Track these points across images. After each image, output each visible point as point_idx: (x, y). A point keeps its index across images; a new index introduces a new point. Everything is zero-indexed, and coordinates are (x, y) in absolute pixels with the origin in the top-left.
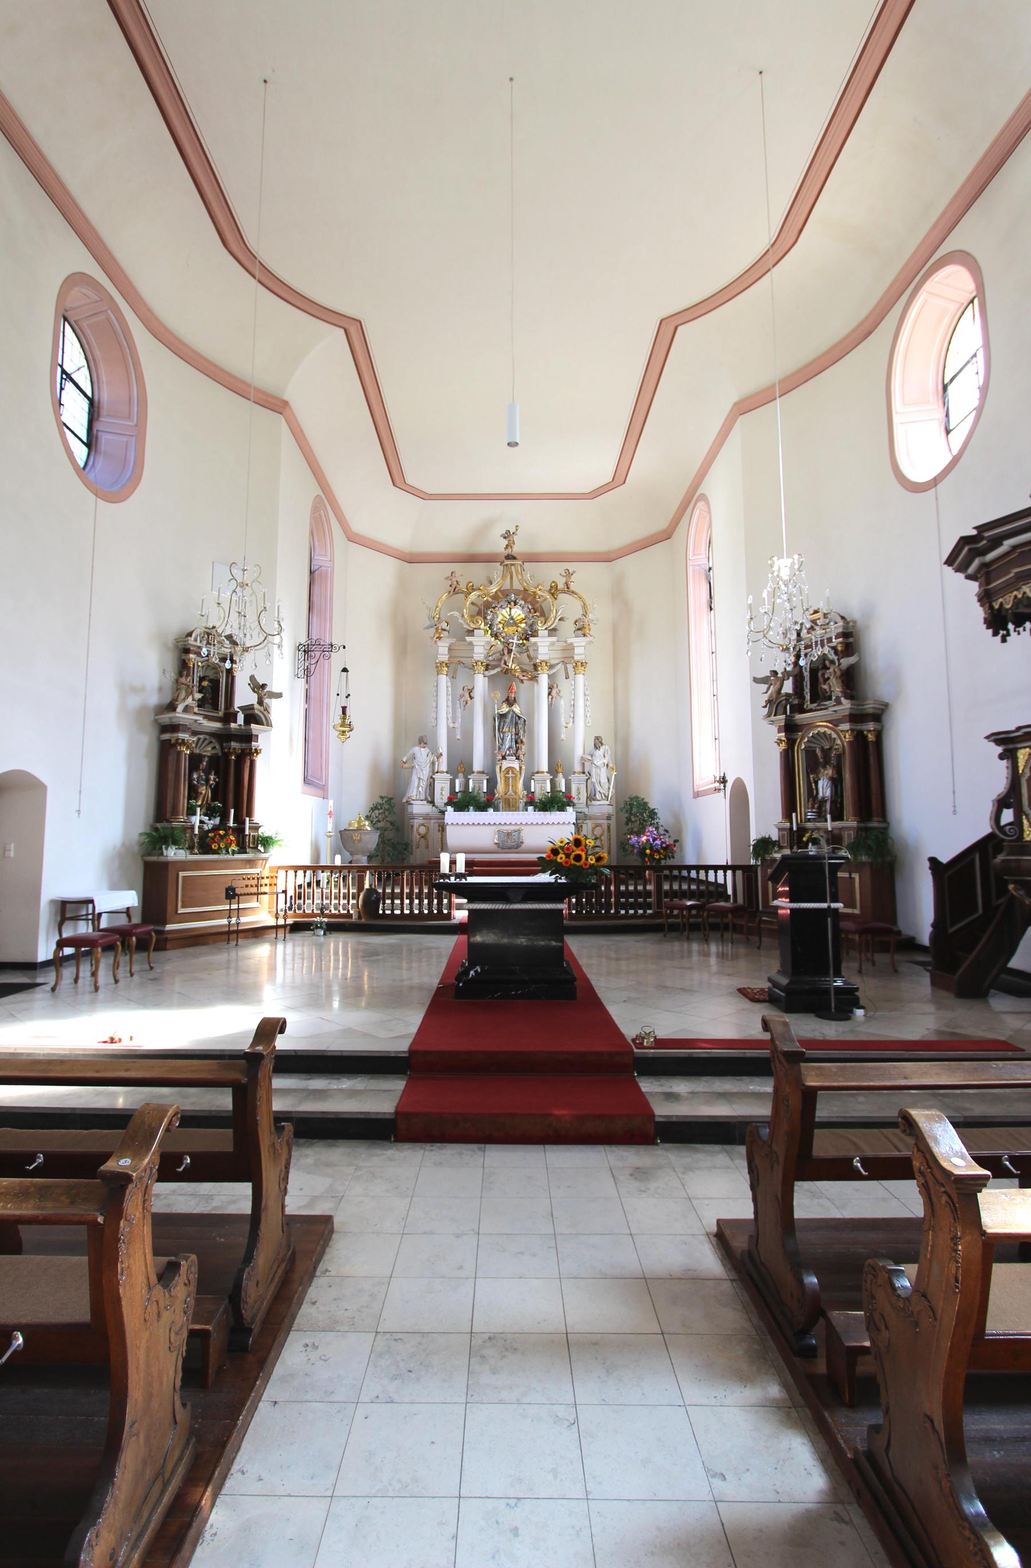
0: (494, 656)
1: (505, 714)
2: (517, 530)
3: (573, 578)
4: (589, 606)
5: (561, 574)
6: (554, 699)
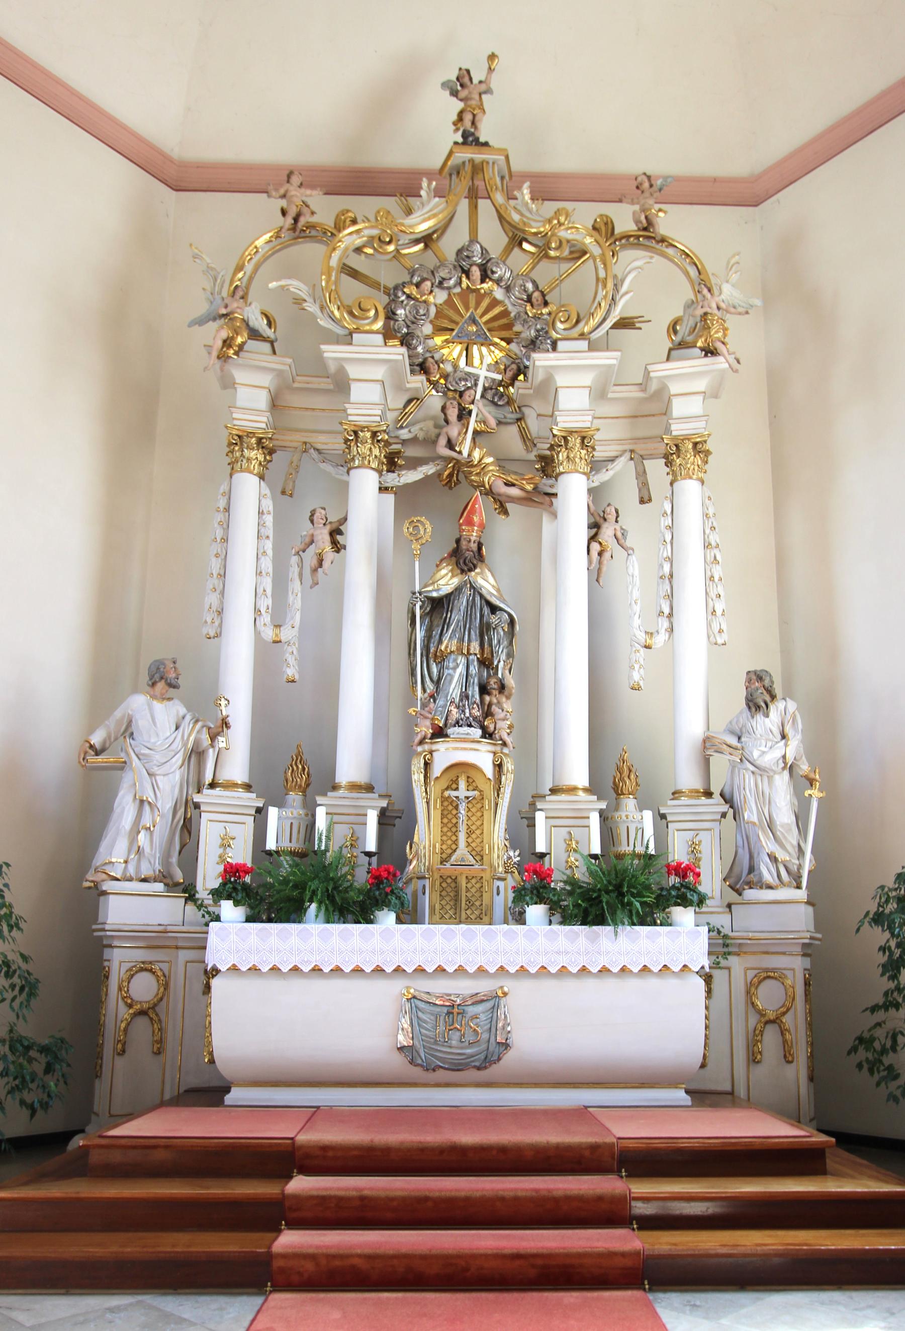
1: (448, 596)
6: (607, 555)
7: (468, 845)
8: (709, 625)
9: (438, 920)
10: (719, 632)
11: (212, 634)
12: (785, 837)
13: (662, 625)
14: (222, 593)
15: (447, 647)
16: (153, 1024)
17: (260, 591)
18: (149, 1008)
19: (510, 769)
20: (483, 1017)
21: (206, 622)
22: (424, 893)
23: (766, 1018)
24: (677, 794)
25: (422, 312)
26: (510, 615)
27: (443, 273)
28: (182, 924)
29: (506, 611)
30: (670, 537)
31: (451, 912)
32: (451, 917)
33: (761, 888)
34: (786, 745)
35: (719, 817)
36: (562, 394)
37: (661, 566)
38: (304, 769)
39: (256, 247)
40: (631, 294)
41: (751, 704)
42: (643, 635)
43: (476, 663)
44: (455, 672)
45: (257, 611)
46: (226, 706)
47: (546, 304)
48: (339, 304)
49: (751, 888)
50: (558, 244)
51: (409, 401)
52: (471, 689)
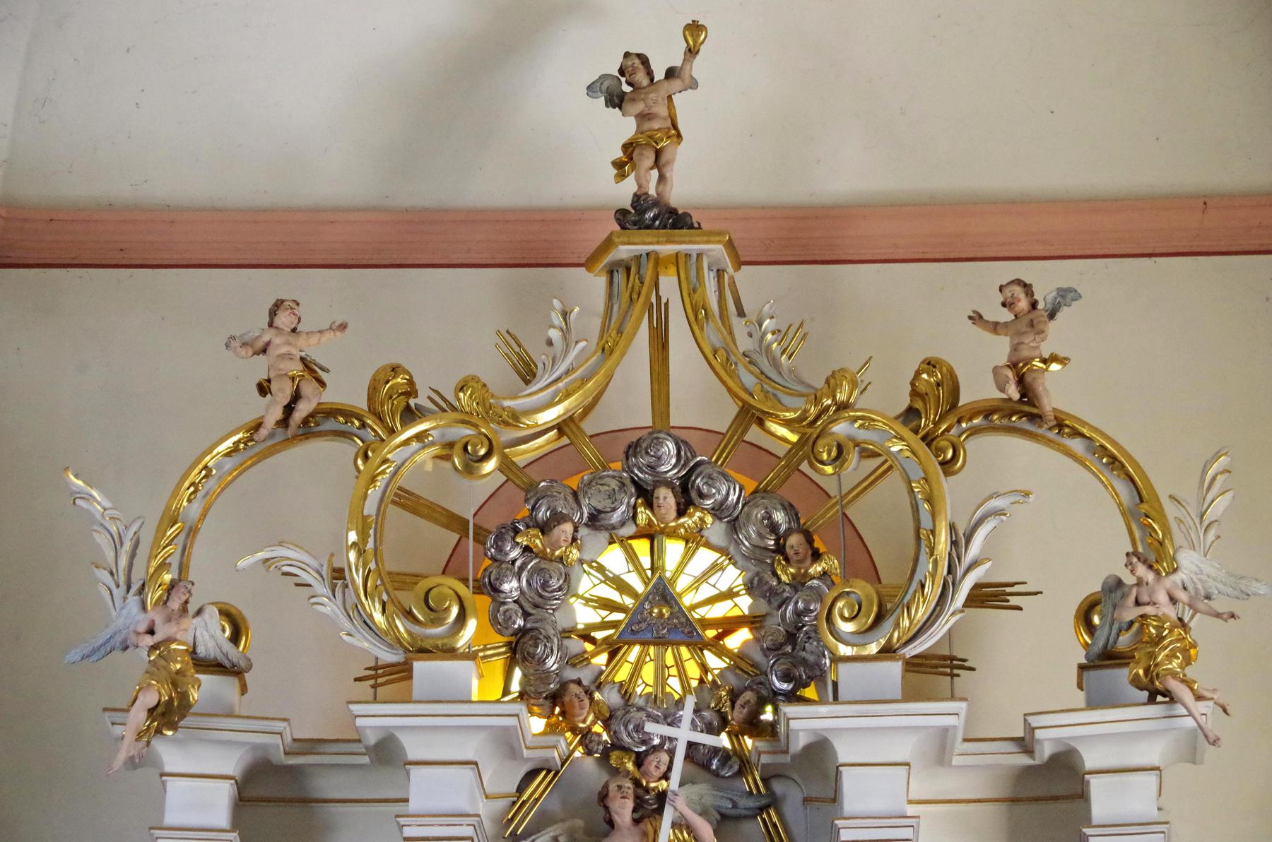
2: (692, 52)
3: (1055, 337)
4: (1170, 510)
5: (976, 318)
25: (555, 583)
27: (599, 502)
39: (206, 467)
40: (988, 565)
48: (385, 597)
50: (834, 454)
51: (531, 775)
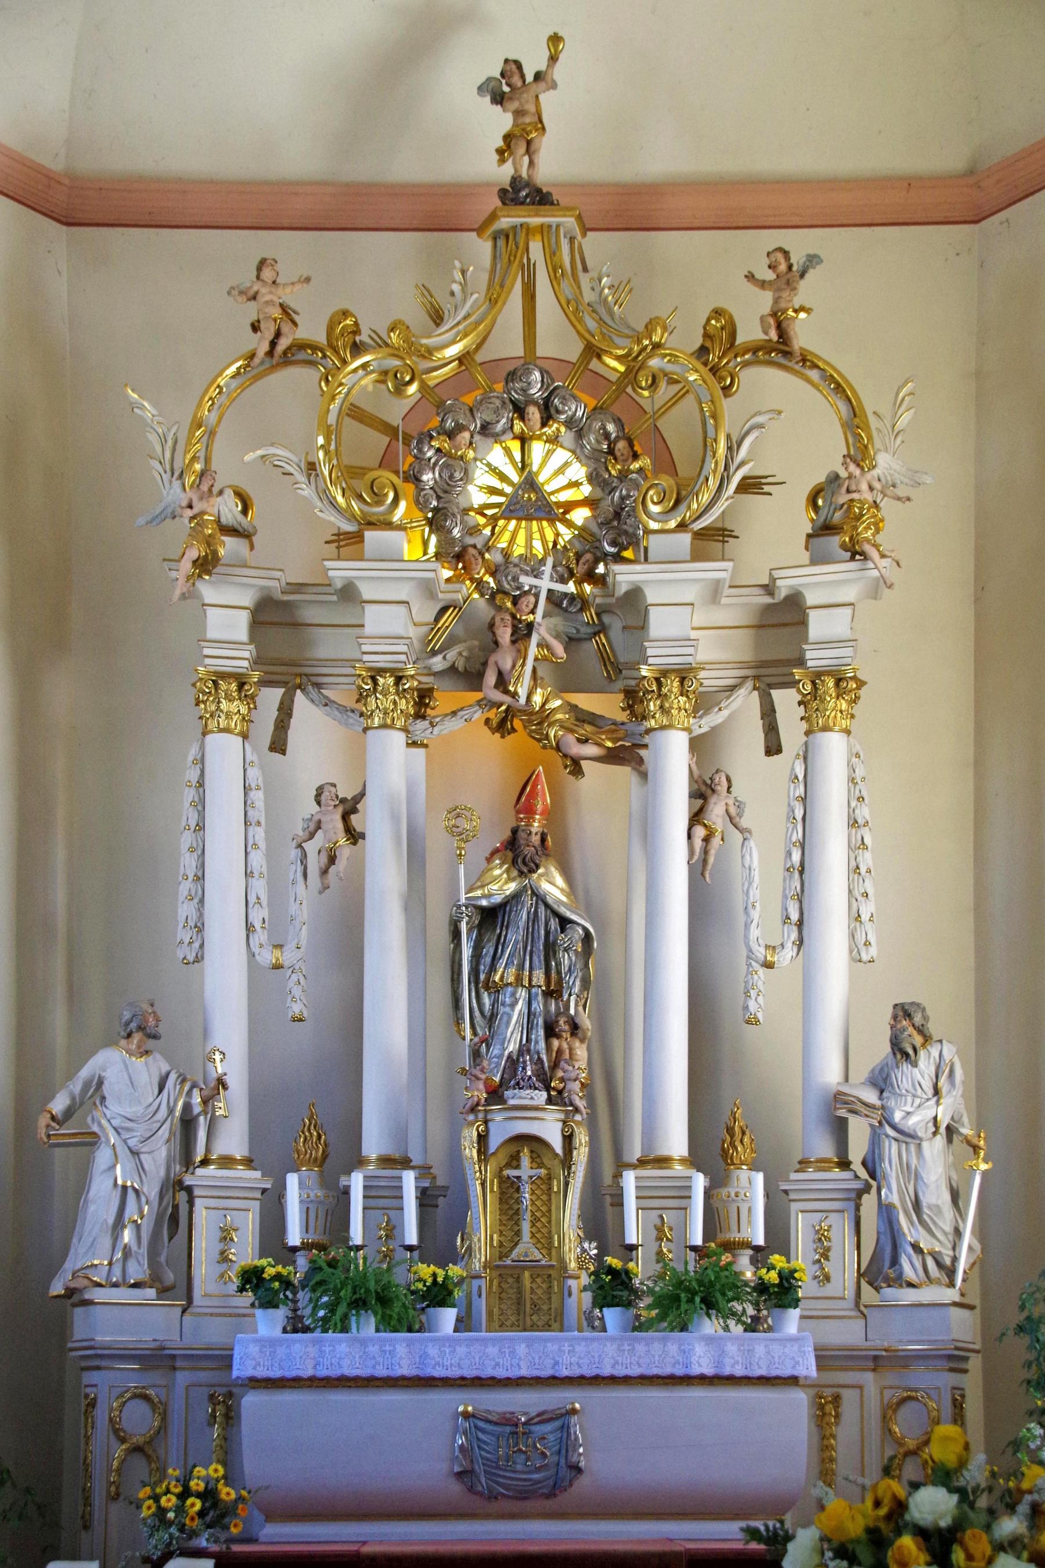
0: (452, 654)
1: (503, 905)
6: (716, 841)
7: (533, 1235)
8: (852, 936)
9: (497, 1327)
10: (865, 944)
11: (191, 958)
12: (935, 1223)
13: (789, 936)
14: (202, 901)
15: (502, 978)
16: (150, 1463)
17: (252, 899)
18: (146, 1443)
19: (583, 1141)
20: (551, 1438)
21: (181, 942)
22: (480, 1296)
23: (905, 1449)
24: (804, 1164)
25: (458, 475)
26: (585, 929)
28: (683, 1211)
29: (578, 924)
30: (802, 812)
31: (513, 1318)
32: (512, 1325)
33: (901, 1286)
34: (938, 1103)
35: (853, 1195)
36: (654, 614)
37: (789, 854)
38: (319, 1137)
39: (218, 386)
41: (896, 1049)
42: (762, 950)
43: (540, 998)
44: (513, 1010)
45: (249, 928)
46: (222, 1061)
47: (635, 456)
49: (889, 1286)
52: (534, 1031)
